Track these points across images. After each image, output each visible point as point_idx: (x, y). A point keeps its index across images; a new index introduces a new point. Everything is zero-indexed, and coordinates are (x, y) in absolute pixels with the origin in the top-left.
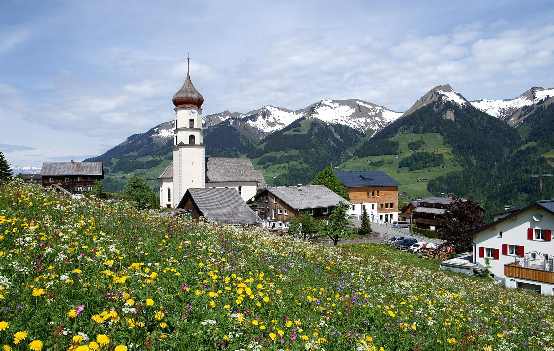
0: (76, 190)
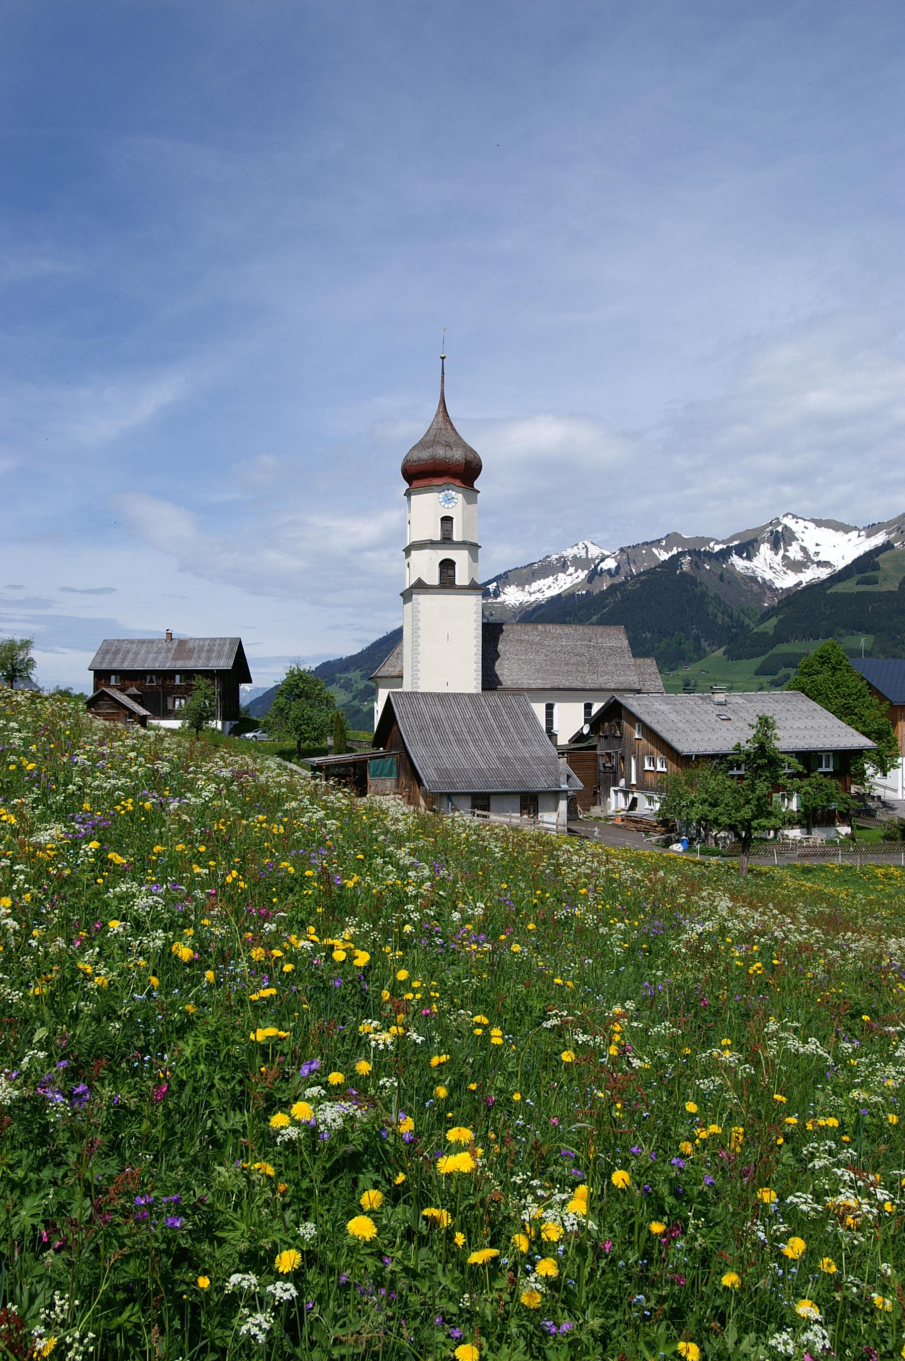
0: (170, 707)
